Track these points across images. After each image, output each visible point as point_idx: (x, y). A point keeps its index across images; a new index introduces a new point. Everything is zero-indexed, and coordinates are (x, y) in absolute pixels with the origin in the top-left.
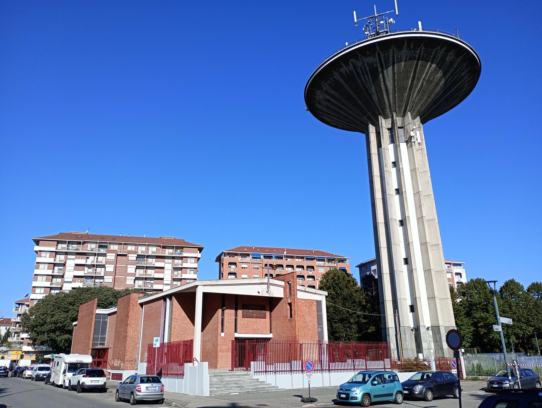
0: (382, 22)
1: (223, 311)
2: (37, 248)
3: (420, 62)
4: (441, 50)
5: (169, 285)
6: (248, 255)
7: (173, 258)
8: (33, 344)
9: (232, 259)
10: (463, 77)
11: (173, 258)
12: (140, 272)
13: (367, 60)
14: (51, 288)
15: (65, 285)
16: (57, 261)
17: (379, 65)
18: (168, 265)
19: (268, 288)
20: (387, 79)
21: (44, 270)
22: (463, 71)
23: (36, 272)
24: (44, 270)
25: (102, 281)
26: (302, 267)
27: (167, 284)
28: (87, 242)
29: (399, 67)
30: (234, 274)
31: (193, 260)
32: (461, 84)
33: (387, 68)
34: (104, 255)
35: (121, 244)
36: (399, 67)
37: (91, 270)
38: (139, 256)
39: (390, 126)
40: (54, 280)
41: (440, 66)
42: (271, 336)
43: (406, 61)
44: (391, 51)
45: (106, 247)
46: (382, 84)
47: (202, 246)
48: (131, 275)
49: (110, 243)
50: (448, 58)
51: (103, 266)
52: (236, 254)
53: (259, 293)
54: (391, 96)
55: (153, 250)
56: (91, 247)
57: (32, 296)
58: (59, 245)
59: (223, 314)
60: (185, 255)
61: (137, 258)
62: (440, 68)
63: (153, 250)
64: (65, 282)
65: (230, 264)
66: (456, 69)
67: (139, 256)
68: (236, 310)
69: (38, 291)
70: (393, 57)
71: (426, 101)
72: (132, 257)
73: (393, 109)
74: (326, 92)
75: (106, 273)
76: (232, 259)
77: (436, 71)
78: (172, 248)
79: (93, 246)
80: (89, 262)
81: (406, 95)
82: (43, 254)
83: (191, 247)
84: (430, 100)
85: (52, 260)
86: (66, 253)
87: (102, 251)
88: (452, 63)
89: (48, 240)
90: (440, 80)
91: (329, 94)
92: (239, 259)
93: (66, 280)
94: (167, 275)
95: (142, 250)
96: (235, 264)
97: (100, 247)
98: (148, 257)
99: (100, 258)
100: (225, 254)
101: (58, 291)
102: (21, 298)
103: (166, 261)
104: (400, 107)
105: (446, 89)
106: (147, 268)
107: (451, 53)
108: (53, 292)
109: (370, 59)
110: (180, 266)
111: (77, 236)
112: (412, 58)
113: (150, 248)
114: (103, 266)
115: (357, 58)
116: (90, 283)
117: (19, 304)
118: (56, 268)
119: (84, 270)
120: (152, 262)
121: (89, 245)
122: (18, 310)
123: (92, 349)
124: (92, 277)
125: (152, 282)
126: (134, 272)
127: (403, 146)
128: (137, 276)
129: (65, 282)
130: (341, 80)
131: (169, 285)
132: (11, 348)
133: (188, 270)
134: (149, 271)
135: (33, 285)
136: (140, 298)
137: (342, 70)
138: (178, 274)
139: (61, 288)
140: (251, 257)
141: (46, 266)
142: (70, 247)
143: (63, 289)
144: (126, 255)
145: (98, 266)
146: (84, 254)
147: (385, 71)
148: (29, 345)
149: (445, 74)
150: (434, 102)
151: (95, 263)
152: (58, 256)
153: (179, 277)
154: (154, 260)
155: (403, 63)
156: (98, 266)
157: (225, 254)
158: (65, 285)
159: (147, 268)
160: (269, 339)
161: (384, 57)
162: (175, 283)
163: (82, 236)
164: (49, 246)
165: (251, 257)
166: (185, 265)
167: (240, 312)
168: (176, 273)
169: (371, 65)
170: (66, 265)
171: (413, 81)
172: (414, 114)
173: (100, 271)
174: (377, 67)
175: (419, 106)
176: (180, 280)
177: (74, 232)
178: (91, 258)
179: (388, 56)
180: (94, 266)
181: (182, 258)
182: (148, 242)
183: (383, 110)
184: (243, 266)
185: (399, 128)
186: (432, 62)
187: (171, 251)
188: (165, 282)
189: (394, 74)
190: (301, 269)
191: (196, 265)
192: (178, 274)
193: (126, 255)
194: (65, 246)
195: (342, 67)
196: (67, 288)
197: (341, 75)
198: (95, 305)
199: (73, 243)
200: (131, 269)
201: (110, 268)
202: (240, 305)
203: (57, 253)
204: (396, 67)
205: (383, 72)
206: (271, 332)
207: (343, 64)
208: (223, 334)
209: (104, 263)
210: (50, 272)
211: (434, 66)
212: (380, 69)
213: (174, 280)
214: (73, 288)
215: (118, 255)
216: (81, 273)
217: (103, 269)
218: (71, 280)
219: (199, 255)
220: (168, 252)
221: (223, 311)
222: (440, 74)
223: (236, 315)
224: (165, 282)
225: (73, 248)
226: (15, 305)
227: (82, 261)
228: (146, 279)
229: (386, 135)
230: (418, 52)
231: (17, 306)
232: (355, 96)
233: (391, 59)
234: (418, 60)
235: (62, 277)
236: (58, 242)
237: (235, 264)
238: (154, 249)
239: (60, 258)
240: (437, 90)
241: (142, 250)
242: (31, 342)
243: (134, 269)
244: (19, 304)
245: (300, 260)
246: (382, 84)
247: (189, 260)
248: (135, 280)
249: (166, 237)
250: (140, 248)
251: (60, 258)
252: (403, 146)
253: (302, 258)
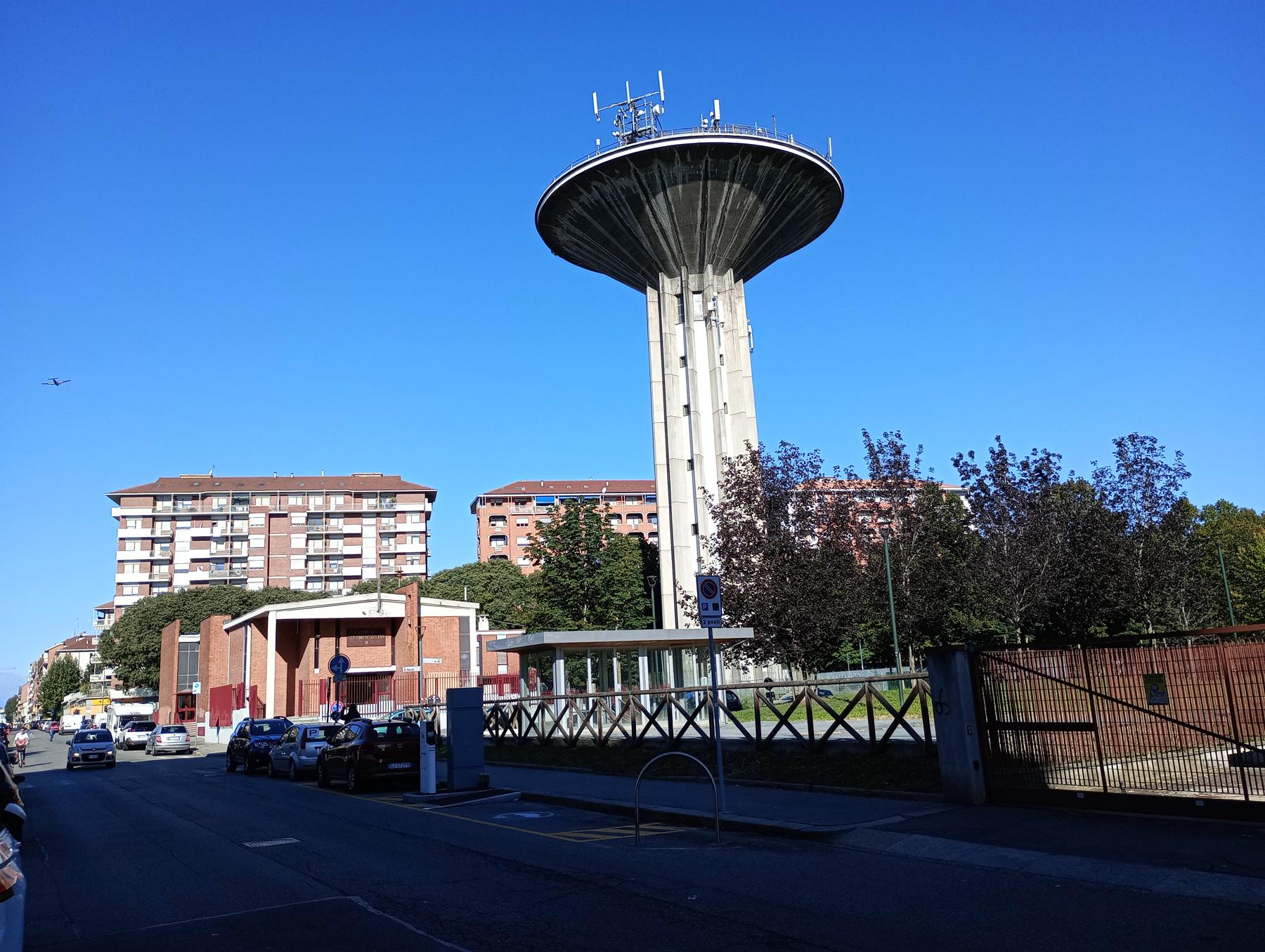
0: (641, 112)
1: (317, 640)
2: (117, 511)
3: (709, 182)
4: (743, 158)
5: (373, 566)
6: (529, 499)
7: (378, 515)
8: (126, 687)
9: (497, 511)
10: (802, 195)
11: (378, 515)
12: (316, 546)
13: (619, 182)
14: (151, 585)
15: (176, 576)
16: (158, 534)
17: (640, 191)
18: (369, 528)
19: (380, 606)
20: (658, 212)
21: (136, 552)
22: (799, 186)
23: (121, 555)
24: (136, 552)
25: (244, 565)
26: (640, 516)
27: (369, 566)
28: (210, 495)
29: (675, 193)
30: (503, 537)
31: (416, 517)
32: (804, 206)
33: (654, 195)
34: (245, 517)
35: (274, 494)
36: (675, 193)
37: (222, 547)
38: (310, 516)
39: (679, 292)
40: (156, 568)
41: (748, 184)
42: (393, 668)
43: (684, 182)
44: (655, 167)
45: (246, 502)
46: (653, 221)
47: (431, 487)
48: (298, 551)
49: (253, 495)
50: (760, 171)
51: (244, 538)
52: (505, 500)
53: (1094, 463)
54: (672, 240)
55: (337, 503)
56: (218, 503)
57: (119, 601)
58: (159, 503)
59: (317, 645)
60: (399, 507)
61: (307, 519)
62: (750, 188)
63: (337, 503)
64: (176, 571)
65: (493, 518)
66: (781, 186)
67: (310, 516)
68: (338, 637)
69: (127, 590)
70: (661, 177)
71: (738, 243)
72: (299, 518)
73: (680, 261)
74: (568, 232)
75: (253, 552)
76: (497, 511)
77: (741, 196)
78: (374, 495)
79: (223, 501)
80: (217, 532)
81: (697, 236)
82: (130, 522)
83: (413, 491)
84: (745, 240)
85: (147, 533)
86: (173, 518)
87: (240, 509)
88: (770, 179)
89: (135, 494)
90: (756, 207)
91: (574, 235)
92: (510, 508)
93: (177, 567)
94: (369, 548)
95: (315, 503)
96: (503, 518)
97: (235, 502)
98: (328, 515)
99: (238, 524)
100: (483, 501)
101: (165, 590)
102: (103, 602)
103: (366, 521)
104: (692, 257)
105: (772, 221)
106: (328, 536)
107: (764, 162)
108: (155, 590)
109: (624, 182)
110: (392, 530)
111: (190, 483)
112: (693, 178)
113: (332, 499)
114: (244, 538)
115: (601, 180)
116: (223, 573)
117: (104, 611)
118: (157, 546)
119: (209, 547)
120: (337, 525)
121: (215, 500)
122: (102, 623)
123: (178, 695)
124: (226, 560)
125: (341, 562)
126: (303, 546)
127: (699, 327)
128: (311, 552)
129: (176, 571)
130: (585, 214)
131: (373, 566)
132: (90, 694)
133: (409, 538)
134: (334, 543)
135: (118, 580)
136: (225, 622)
137: (582, 199)
138: (391, 545)
139: (170, 584)
140: (535, 502)
141: (138, 544)
142: (180, 506)
143: (175, 583)
144: (285, 515)
145: (233, 539)
146: (207, 517)
147: (653, 201)
148: (117, 688)
149: (761, 197)
150: (756, 242)
151: (229, 534)
152: (158, 524)
153: (392, 550)
154: (341, 520)
155: (680, 187)
156: (233, 539)
157: (483, 501)
158: (176, 576)
159: (328, 536)
160: (391, 673)
161: (646, 177)
162: (385, 562)
163: (202, 482)
164: (140, 505)
165: (535, 502)
166: (401, 528)
167: (343, 640)
168: (385, 543)
169: (627, 191)
170: (176, 539)
171: (704, 214)
172: (720, 266)
173: (241, 548)
174: (638, 195)
175: (726, 253)
176: (395, 555)
177: (185, 474)
178: (222, 524)
179: (652, 175)
180: (227, 538)
181: (395, 514)
182: (328, 487)
183: (664, 262)
184: (520, 521)
185: (694, 293)
186: (732, 181)
187: (373, 501)
188: (365, 562)
189: (668, 204)
190: (636, 521)
191: (422, 527)
192: (391, 545)
193: (285, 515)
194: (169, 504)
195: (581, 193)
196: (182, 582)
197: (582, 204)
198: (177, 630)
199: (184, 498)
200: (298, 541)
201: (258, 541)
202: (343, 630)
203: (155, 519)
204: (669, 193)
205: (649, 202)
206: (393, 663)
207: (581, 190)
208: (317, 671)
209: (245, 532)
210: (146, 555)
211: (736, 186)
212: (643, 198)
213: (382, 556)
214: (193, 582)
215: (271, 516)
216: (204, 554)
217: (245, 544)
218: (187, 567)
219: (428, 507)
220: (366, 505)
221: (317, 640)
222: (752, 198)
223: (337, 644)
224: (365, 562)
225: (185, 507)
226: (96, 614)
227: (204, 531)
228: (327, 557)
229: (672, 305)
230: (702, 166)
231: (101, 615)
232: (613, 240)
233: (658, 181)
234: (706, 179)
235: (171, 562)
236: (156, 498)
237: (503, 518)
238: (340, 500)
239: (163, 528)
240: (756, 222)
241: (315, 503)
242: (121, 682)
243: (304, 541)
244: (104, 611)
245: (635, 503)
246: (653, 221)
247: (408, 517)
248: (306, 561)
249: (364, 472)
250: (312, 499)
251: (163, 528)
252: (699, 327)
253: (639, 498)
